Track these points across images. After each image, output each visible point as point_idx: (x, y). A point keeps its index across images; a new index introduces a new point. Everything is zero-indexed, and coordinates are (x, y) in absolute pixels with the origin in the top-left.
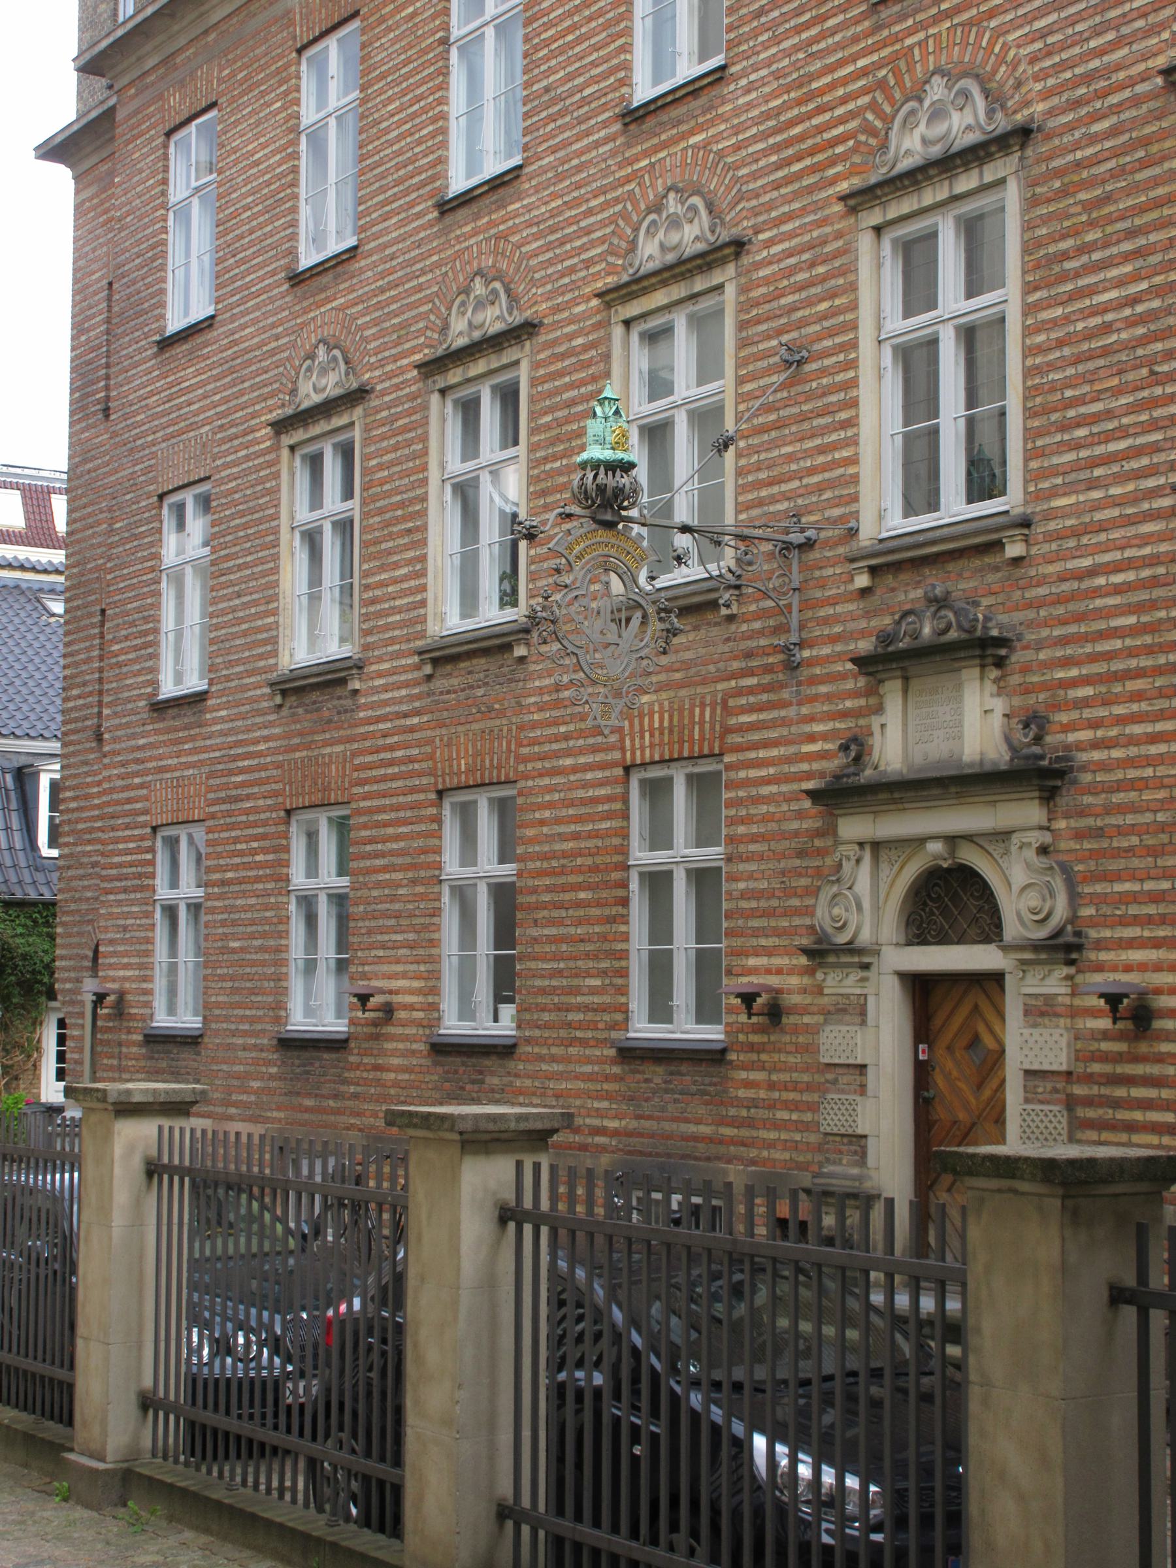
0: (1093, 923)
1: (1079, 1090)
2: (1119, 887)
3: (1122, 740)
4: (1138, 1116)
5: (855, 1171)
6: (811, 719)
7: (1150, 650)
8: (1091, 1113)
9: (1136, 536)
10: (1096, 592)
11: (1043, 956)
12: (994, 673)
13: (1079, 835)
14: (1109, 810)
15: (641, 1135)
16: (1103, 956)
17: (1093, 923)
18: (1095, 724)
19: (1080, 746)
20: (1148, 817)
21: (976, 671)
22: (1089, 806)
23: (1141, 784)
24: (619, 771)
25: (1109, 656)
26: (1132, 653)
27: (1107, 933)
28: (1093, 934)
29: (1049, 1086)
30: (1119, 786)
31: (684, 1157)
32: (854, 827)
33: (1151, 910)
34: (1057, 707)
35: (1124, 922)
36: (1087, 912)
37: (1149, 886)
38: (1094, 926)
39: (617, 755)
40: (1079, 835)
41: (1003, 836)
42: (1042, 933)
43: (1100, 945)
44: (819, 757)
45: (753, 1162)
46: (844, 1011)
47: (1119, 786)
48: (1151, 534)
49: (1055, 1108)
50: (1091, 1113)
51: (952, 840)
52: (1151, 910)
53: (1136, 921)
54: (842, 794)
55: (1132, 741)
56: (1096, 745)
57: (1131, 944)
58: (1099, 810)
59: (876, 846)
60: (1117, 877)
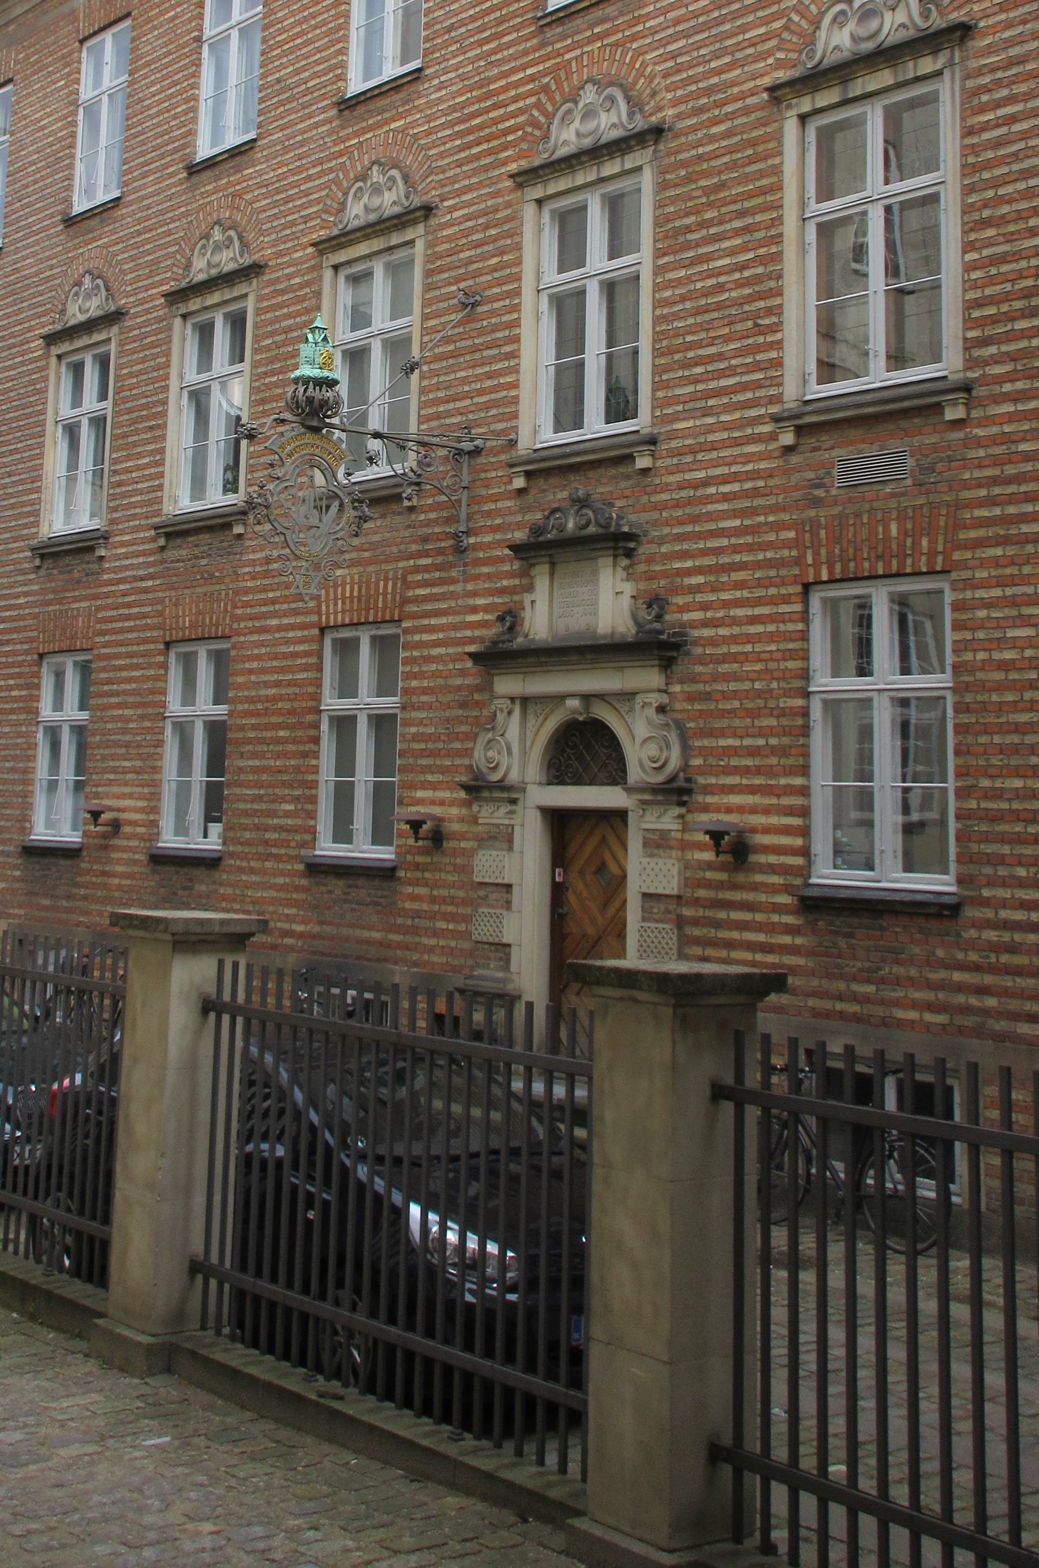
0: (702, 771)
1: (687, 912)
2: (722, 742)
3: (727, 621)
4: (735, 935)
5: (500, 975)
6: (474, 594)
7: (750, 548)
8: (697, 932)
9: (741, 455)
10: (710, 499)
11: (660, 798)
12: (624, 562)
13: (691, 698)
14: (716, 678)
15: (322, 938)
16: (709, 799)
17: (702, 771)
18: (705, 607)
19: (693, 624)
20: (747, 685)
21: (610, 560)
22: (700, 674)
23: (742, 658)
24: (316, 632)
25: (718, 551)
26: (736, 549)
27: (712, 780)
28: (701, 780)
29: (662, 907)
30: (725, 658)
31: (358, 958)
32: (507, 685)
33: (749, 762)
34: (675, 591)
35: (727, 771)
36: (697, 762)
37: (747, 742)
38: (703, 774)
39: (314, 618)
40: (691, 698)
41: (629, 696)
42: (660, 778)
43: (707, 790)
44: (479, 625)
45: (416, 964)
46: (494, 838)
47: (725, 658)
48: (753, 454)
49: (667, 926)
50: (697, 932)
51: (587, 698)
52: (749, 762)
53: (736, 770)
54: (500, 656)
55: (736, 621)
56: (705, 624)
57: (732, 789)
58: (707, 677)
59: (525, 701)
60: (721, 733)
